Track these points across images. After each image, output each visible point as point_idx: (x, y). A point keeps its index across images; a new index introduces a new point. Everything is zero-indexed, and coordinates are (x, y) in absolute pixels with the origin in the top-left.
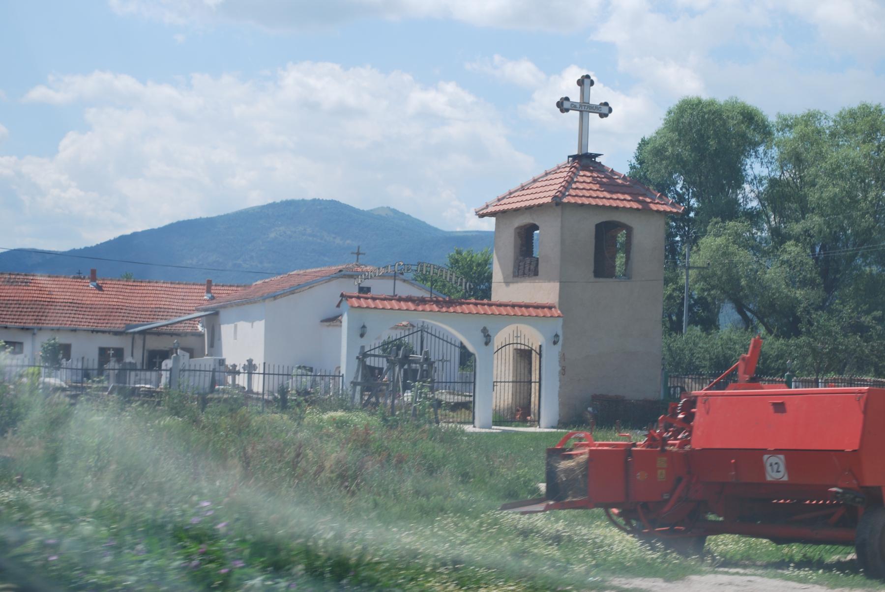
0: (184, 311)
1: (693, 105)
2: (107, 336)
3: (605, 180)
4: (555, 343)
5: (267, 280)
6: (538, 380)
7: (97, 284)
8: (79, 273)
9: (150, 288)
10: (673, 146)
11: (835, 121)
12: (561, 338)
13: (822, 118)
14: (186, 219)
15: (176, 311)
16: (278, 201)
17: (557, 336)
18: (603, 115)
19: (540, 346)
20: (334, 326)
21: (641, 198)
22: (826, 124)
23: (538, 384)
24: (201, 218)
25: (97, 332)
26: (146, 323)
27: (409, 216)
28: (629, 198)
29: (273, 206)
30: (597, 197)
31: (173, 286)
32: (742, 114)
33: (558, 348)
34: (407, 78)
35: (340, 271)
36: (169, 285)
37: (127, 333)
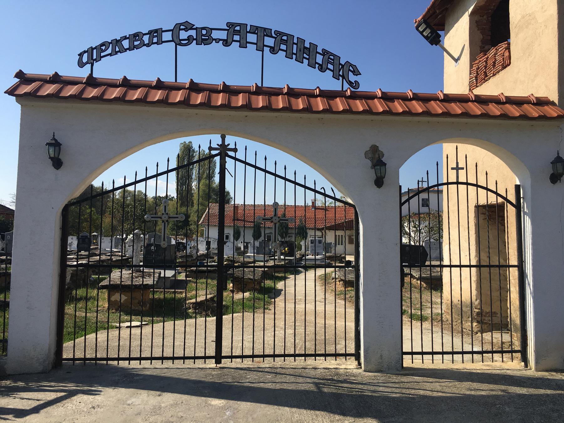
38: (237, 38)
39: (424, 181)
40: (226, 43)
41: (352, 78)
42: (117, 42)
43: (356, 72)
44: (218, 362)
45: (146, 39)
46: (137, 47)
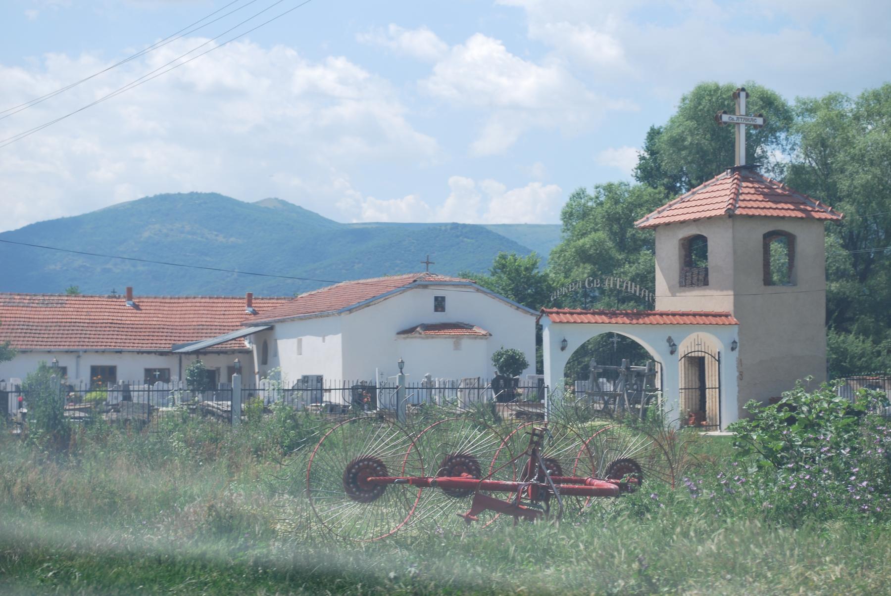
0: (227, 328)
1: (710, 91)
2: (153, 356)
3: (765, 190)
4: (733, 349)
5: (313, 293)
6: (717, 386)
7: (134, 303)
8: (114, 292)
9: (188, 304)
10: (692, 134)
11: (857, 104)
13: (844, 101)
14: (46, 219)
15: (219, 327)
16: (151, 195)
17: (735, 342)
19: (719, 353)
20: (412, 338)
21: (802, 207)
22: (849, 108)
23: (717, 390)
24: (63, 219)
25: (143, 352)
26: (190, 342)
27: (300, 207)
28: (792, 207)
29: (146, 200)
30: (764, 208)
31: (211, 301)
32: (762, 99)
33: (736, 353)
34: (291, 53)
35: (415, 281)
36: (208, 300)
37: (173, 353)
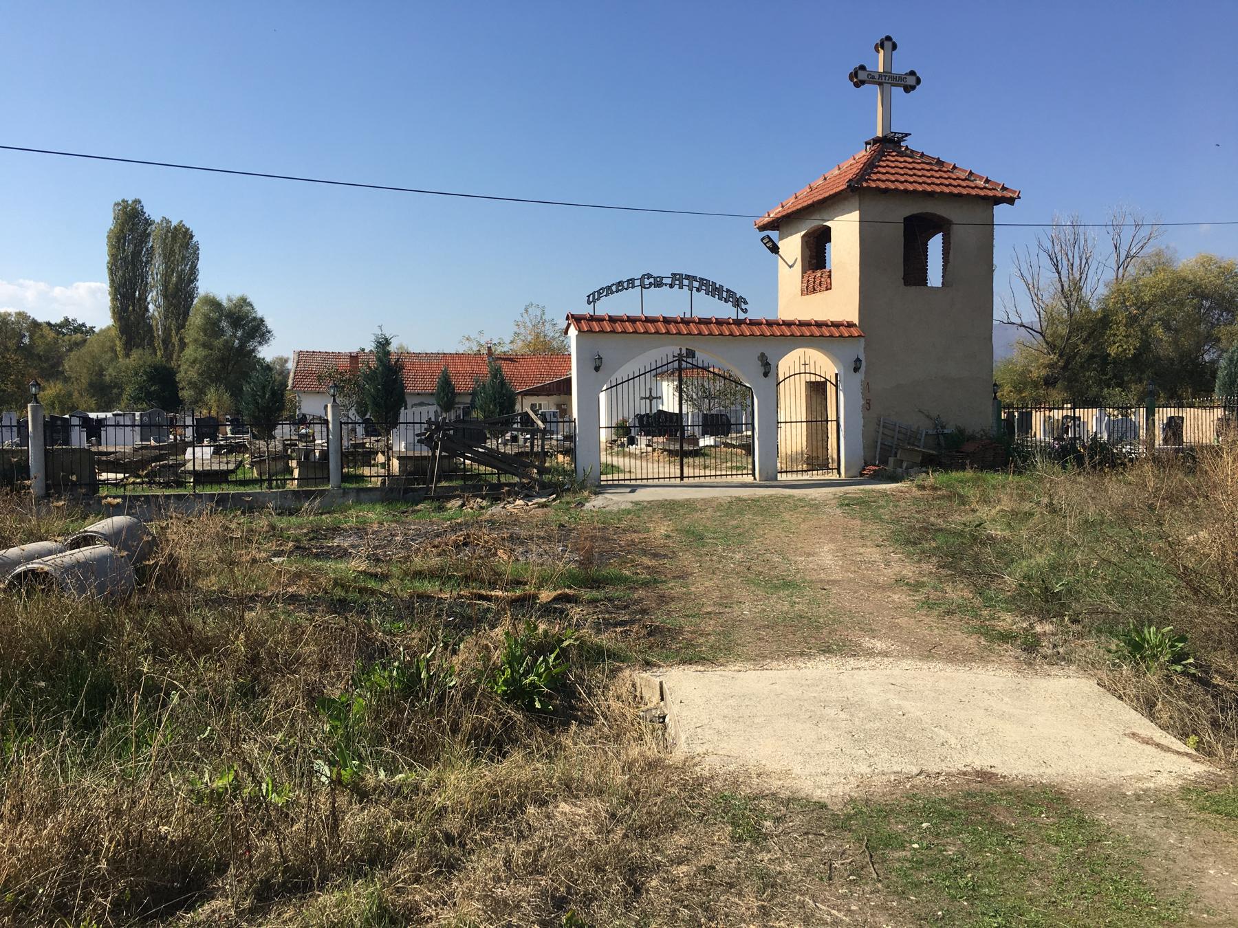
4: (856, 370)
12: (864, 364)
17: (858, 360)
18: (908, 89)
33: (860, 376)
38: (677, 282)
39: (648, 398)
40: (671, 286)
41: (743, 306)
42: (609, 288)
43: (746, 303)
44: (682, 479)
45: (625, 285)
46: (621, 290)
